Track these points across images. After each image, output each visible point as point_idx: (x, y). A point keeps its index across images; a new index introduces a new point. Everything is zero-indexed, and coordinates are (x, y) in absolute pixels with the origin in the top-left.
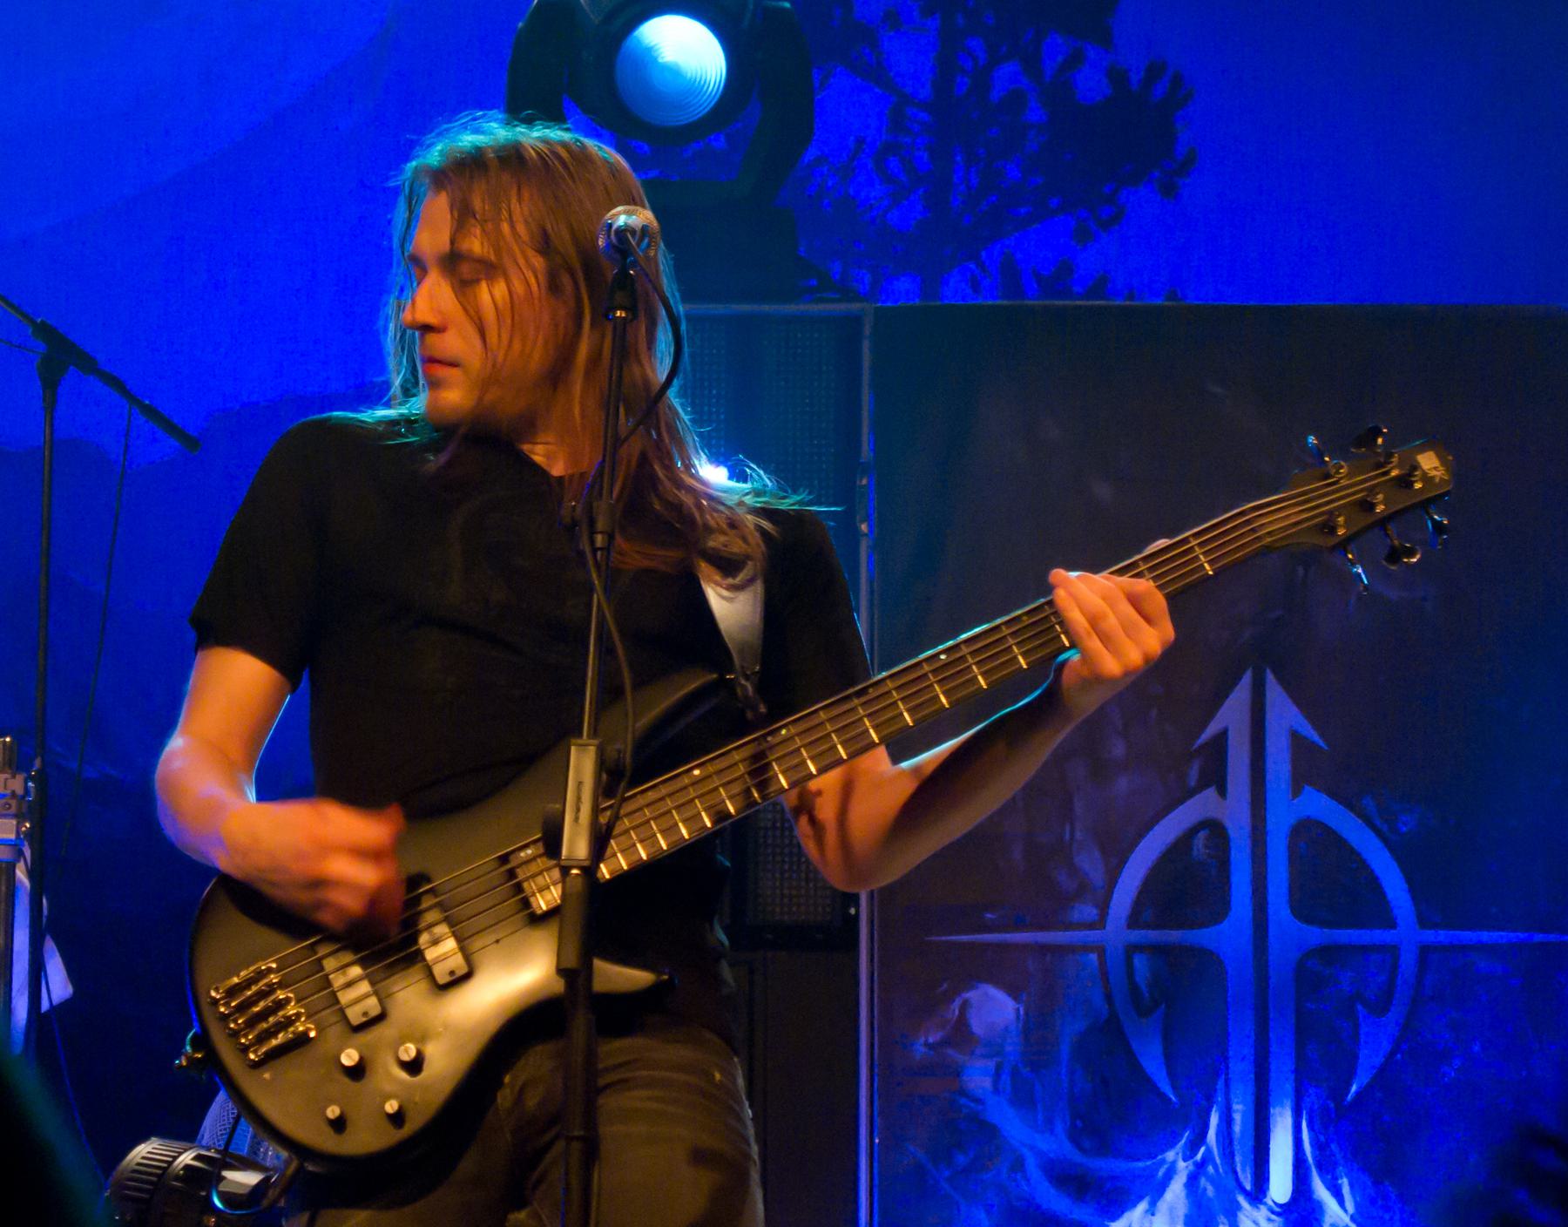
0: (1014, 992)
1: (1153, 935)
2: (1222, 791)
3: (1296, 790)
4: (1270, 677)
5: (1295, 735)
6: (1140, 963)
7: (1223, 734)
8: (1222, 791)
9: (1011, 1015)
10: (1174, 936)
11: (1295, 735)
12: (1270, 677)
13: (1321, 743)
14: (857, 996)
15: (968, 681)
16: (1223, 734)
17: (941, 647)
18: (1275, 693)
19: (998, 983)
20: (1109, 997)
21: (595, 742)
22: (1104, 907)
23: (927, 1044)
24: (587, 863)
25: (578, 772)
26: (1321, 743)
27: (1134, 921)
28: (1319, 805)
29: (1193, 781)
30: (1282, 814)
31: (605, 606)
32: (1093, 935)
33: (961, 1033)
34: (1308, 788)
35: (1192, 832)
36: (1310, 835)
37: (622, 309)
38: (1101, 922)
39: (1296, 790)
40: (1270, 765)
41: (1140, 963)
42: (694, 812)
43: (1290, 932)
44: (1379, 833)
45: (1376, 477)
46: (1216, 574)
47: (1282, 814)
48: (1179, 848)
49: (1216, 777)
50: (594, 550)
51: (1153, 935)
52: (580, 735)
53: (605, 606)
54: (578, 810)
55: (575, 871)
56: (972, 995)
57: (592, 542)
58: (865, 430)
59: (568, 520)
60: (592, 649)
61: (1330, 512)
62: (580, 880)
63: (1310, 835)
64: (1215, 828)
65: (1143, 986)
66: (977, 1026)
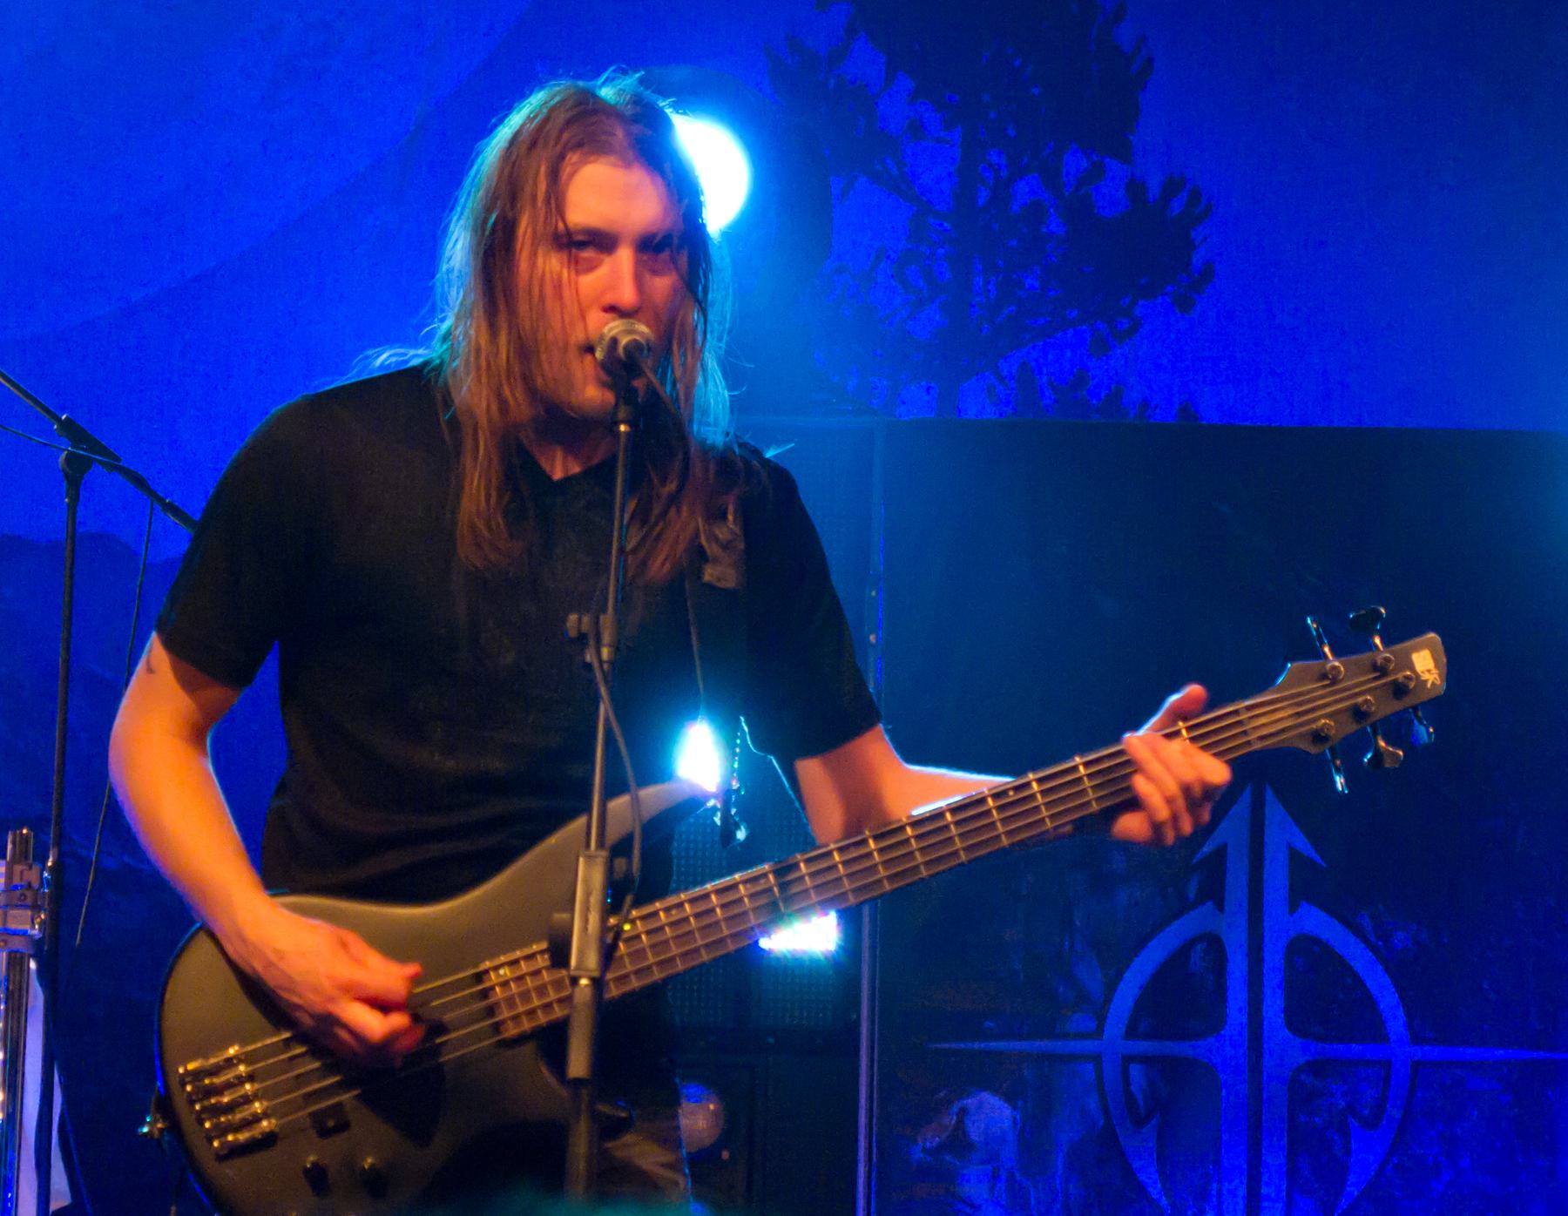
0: (1010, 1098)
1: (1143, 1046)
2: (1220, 906)
3: (1293, 907)
4: (1270, 795)
5: (1294, 854)
6: (1136, 1071)
7: (1221, 852)
9: (1007, 1124)
10: (1168, 1047)
11: (1294, 854)
12: (1270, 795)
13: (1317, 857)
14: (856, 1122)
15: (1123, 789)
16: (1221, 852)
17: (503, 959)
18: (1274, 809)
19: (996, 1092)
20: (1106, 1111)
22: (1102, 1019)
23: (925, 1150)
24: (596, 974)
26: (1317, 857)
27: (1131, 1032)
28: (1317, 922)
29: (1192, 891)
31: (615, 725)
32: (1089, 1045)
33: (959, 1142)
35: (1189, 945)
38: (1100, 1030)
39: (1293, 907)
41: (1136, 1071)
42: (737, 896)
43: (1285, 1047)
45: (1376, 679)
48: (1181, 955)
49: (1214, 892)
50: (601, 662)
51: (1143, 1046)
53: (615, 725)
56: (970, 1102)
58: (862, 1169)
64: (1214, 943)
65: (1140, 1097)
66: (975, 1133)
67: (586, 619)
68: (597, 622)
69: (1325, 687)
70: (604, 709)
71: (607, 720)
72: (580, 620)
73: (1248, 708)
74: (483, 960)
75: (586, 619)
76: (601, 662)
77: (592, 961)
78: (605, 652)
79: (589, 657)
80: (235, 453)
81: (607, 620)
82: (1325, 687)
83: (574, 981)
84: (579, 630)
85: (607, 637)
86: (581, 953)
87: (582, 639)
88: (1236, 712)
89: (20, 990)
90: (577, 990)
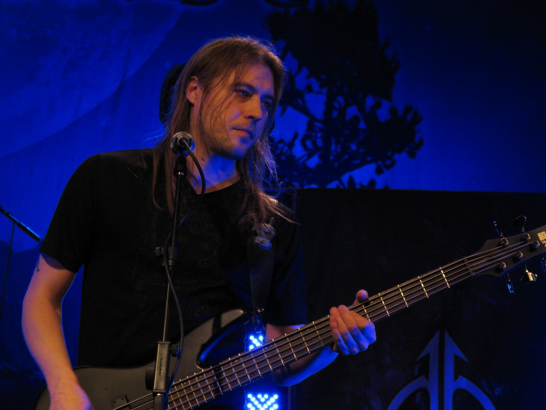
2: (427, 378)
3: (456, 378)
4: (446, 334)
5: (457, 358)
7: (428, 356)
8: (427, 378)
11: (457, 358)
12: (446, 334)
16: (428, 356)
21: (168, 343)
24: (164, 391)
25: (160, 354)
28: (464, 383)
30: (452, 384)
34: (460, 377)
36: (459, 393)
37: (180, 171)
39: (456, 378)
40: (445, 403)
44: (487, 394)
45: (521, 244)
46: (274, 370)
47: (452, 384)
48: (411, 398)
49: (425, 372)
50: (169, 266)
52: (162, 340)
54: (161, 370)
55: (159, 394)
57: (168, 263)
59: (158, 255)
60: (167, 306)
61: (500, 262)
62: (161, 398)
63: (459, 393)
67: (163, 249)
68: (167, 251)
69: (499, 249)
70: (170, 285)
71: (170, 289)
72: (160, 249)
73: (469, 259)
74: (289, 223)
75: (163, 249)
76: (169, 266)
77: (162, 386)
78: (170, 261)
79: (164, 264)
80: (203, 54)
81: (172, 249)
82: (499, 249)
83: (155, 394)
84: (160, 253)
85: (171, 257)
86: (158, 382)
87: (161, 256)
88: (463, 261)
89: (208, 152)
90: (156, 397)
